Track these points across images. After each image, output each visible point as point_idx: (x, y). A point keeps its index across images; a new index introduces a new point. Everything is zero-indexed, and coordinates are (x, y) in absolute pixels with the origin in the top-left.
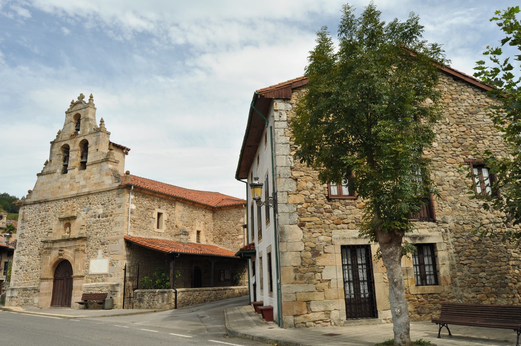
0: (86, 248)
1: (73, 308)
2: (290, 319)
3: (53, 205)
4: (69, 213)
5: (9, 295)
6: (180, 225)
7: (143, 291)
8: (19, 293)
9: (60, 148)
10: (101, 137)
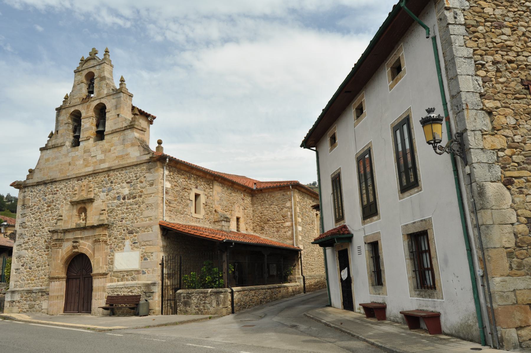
0: (108, 239)
1: (95, 314)
2: (512, 334)
3: (62, 186)
4: (84, 195)
5: (9, 299)
6: (219, 210)
7: (190, 291)
8: (22, 297)
9: (68, 115)
10: (122, 99)
